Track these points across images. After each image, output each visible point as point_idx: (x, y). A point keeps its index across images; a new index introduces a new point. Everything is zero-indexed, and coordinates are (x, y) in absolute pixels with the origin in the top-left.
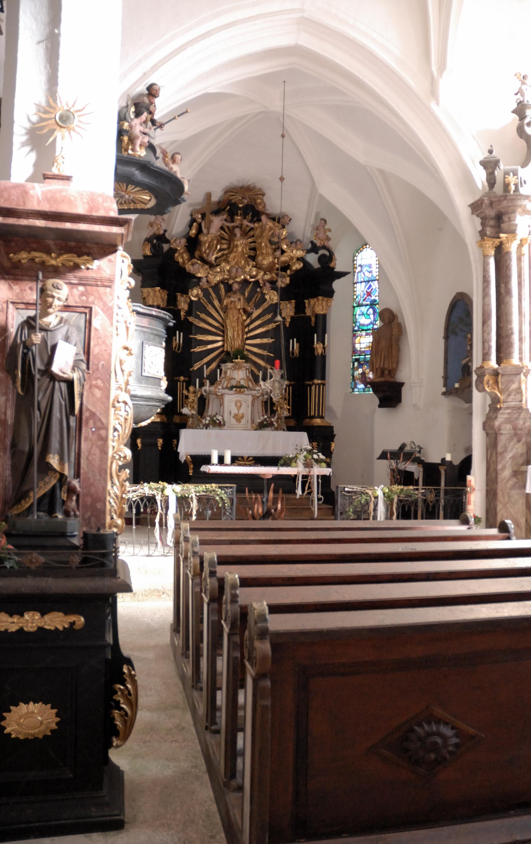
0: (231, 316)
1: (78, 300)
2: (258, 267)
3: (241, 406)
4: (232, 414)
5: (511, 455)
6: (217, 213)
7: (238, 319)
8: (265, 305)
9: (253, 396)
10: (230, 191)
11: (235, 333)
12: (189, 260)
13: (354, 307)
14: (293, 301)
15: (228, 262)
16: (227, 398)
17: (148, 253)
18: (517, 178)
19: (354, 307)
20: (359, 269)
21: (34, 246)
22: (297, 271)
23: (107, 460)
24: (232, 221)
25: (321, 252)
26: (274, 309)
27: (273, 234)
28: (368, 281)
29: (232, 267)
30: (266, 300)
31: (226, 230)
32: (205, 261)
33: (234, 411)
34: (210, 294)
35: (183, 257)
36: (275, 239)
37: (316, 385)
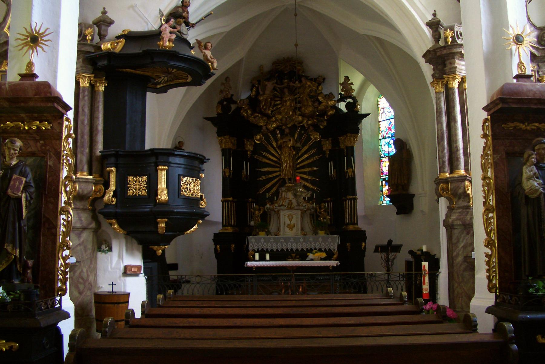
0: (284, 153)
1: (40, 149)
2: (303, 115)
3: (292, 218)
4: (286, 225)
5: (462, 245)
6: (268, 80)
7: (289, 154)
8: (310, 143)
9: (302, 210)
10: (277, 63)
11: (288, 165)
12: (252, 115)
13: (380, 139)
14: (330, 138)
15: (280, 113)
16: (282, 213)
17: (220, 111)
18: (454, 33)
19: (380, 139)
20: (382, 110)
21: (15, 118)
22: (332, 116)
23: (56, 249)
24: (282, 84)
25: (349, 100)
26: (318, 145)
27: (310, 91)
28: (389, 119)
29: (283, 117)
30: (311, 139)
31: (278, 90)
32: (264, 115)
33: (288, 222)
34: (270, 138)
35: (247, 113)
36: (313, 94)
37: (349, 199)
